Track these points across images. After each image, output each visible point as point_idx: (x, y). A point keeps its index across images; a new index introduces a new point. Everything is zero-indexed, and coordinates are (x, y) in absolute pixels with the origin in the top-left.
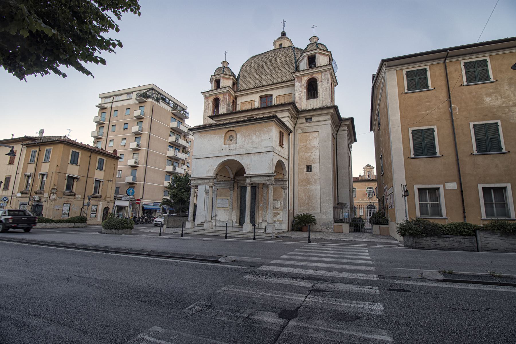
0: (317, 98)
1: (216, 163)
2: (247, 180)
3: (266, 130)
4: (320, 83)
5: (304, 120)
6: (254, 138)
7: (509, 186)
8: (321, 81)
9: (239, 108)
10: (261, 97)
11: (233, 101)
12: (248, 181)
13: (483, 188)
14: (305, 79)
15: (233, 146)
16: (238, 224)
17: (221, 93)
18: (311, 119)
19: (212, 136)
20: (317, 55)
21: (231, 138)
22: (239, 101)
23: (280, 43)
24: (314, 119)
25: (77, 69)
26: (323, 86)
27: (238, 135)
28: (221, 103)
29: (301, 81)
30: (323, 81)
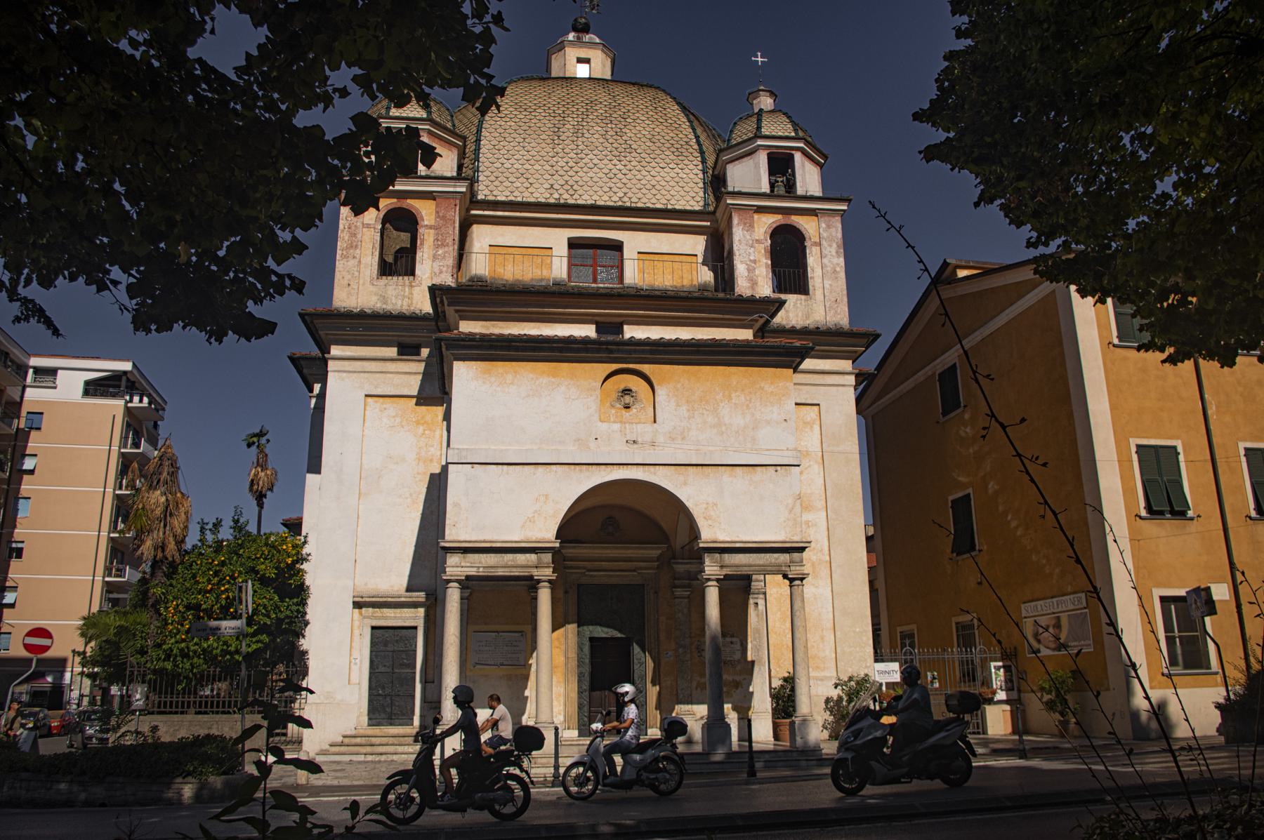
1: (568, 490)
2: (707, 561)
3: (768, 388)
4: (815, 250)
6: (725, 410)
7: (954, 620)
8: (820, 244)
10: (573, 244)
12: (711, 568)
14: (765, 223)
15: (643, 430)
16: (575, 733)
19: (545, 380)
21: (627, 399)
26: (825, 261)
27: (661, 392)
29: (750, 227)
30: (824, 242)
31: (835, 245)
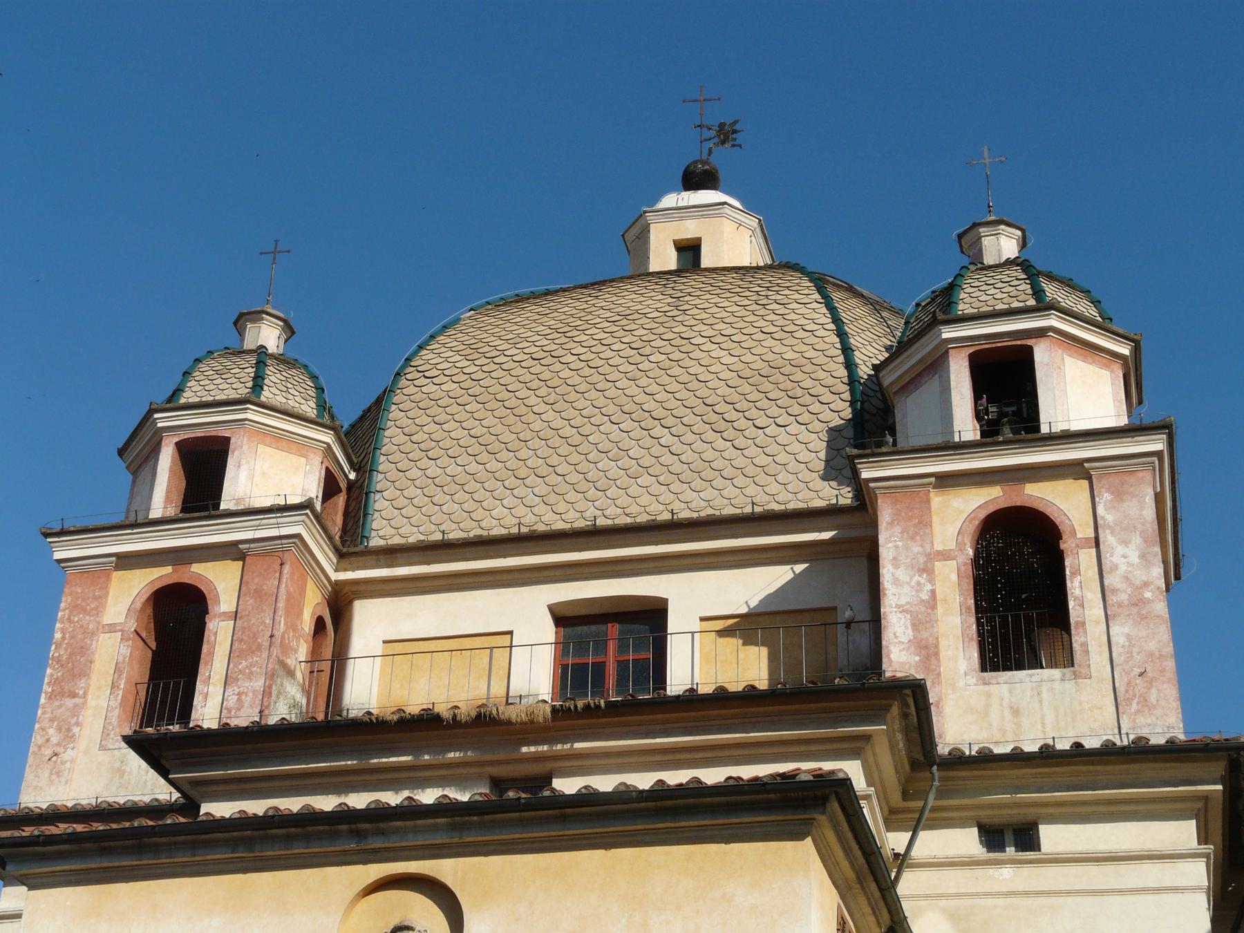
0: (1065, 658)
5: (966, 841)
9: (365, 691)
10: (563, 618)
11: (320, 624)
13: (552, 609)
14: (971, 504)
17: (232, 551)
18: (1026, 838)
20: (1042, 354)
22: (373, 622)
23: (689, 229)
24: (1052, 836)
25: (31, 888)
28: (219, 634)
31: (1137, 540)
